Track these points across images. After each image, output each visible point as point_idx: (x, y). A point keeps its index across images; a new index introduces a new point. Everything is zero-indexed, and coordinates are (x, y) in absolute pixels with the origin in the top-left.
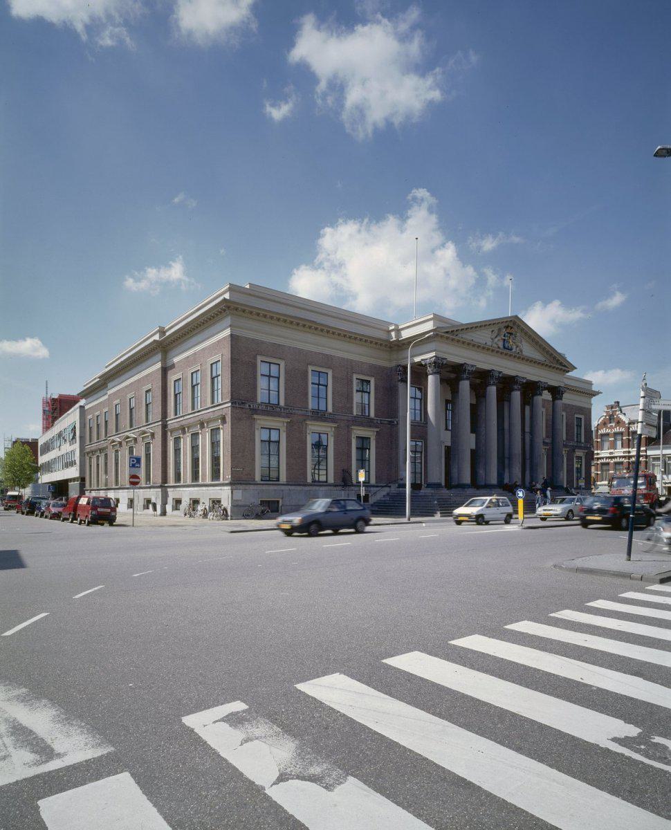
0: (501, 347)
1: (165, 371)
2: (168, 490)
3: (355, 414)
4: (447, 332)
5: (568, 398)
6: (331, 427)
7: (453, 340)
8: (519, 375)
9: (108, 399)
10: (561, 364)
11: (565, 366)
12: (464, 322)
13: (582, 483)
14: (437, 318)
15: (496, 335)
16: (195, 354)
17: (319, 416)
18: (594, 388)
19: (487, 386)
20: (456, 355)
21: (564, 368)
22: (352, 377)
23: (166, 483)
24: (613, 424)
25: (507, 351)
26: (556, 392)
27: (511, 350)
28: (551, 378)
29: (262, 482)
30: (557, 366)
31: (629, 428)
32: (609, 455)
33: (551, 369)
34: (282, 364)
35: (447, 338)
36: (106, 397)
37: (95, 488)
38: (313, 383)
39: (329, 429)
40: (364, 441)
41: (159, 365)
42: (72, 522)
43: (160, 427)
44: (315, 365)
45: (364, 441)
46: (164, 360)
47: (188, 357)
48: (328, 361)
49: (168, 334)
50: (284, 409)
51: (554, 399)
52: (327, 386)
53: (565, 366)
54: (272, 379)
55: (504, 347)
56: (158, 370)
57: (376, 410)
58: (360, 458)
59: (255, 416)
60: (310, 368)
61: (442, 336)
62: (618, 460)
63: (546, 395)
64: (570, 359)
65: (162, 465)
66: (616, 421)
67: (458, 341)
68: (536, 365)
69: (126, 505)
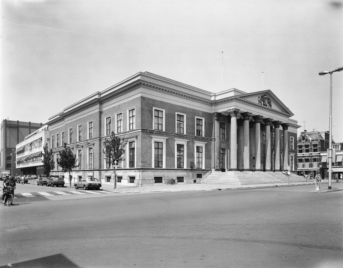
0: (262, 104)
1: (101, 113)
2: (102, 171)
3: (176, 132)
4: (240, 97)
5: (290, 129)
6: (186, 141)
7: (242, 101)
8: (270, 118)
9: (65, 126)
10: (287, 113)
11: (289, 114)
12: (248, 92)
13: (300, 168)
14: (235, 90)
15: (260, 99)
16: (119, 105)
17: (180, 136)
18: (298, 124)
19: (257, 123)
20: (244, 108)
21: (289, 115)
22: (195, 117)
23: (101, 168)
24: (304, 141)
25: (265, 106)
26: (285, 126)
27: (267, 106)
28: (283, 120)
29: (178, 169)
30: (283, 113)
31: (311, 143)
32: (309, 155)
33: (263, 109)
34: (164, 111)
35: (240, 100)
36: (64, 125)
37: (56, 170)
38: (177, 121)
39: (163, 140)
40: (180, 146)
41: (98, 110)
42: (53, 187)
43: (99, 140)
44: (178, 112)
45: (180, 146)
46: (100, 108)
47: (115, 107)
48: (184, 110)
49: (102, 96)
50: (165, 132)
51: (284, 129)
52: (162, 118)
53: (289, 114)
54: (200, 126)
55: (264, 105)
56: (97, 113)
57: (205, 134)
58: (198, 157)
59: (152, 136)
60: (176, 113)
61: (238, 99)
62: (307, 158)
63: (281, 128)
64: (291, 109)
65: (99, 159)
66: (305, 139)
67: (245, 101)
68: (254, 106)
69: (136, 179)
